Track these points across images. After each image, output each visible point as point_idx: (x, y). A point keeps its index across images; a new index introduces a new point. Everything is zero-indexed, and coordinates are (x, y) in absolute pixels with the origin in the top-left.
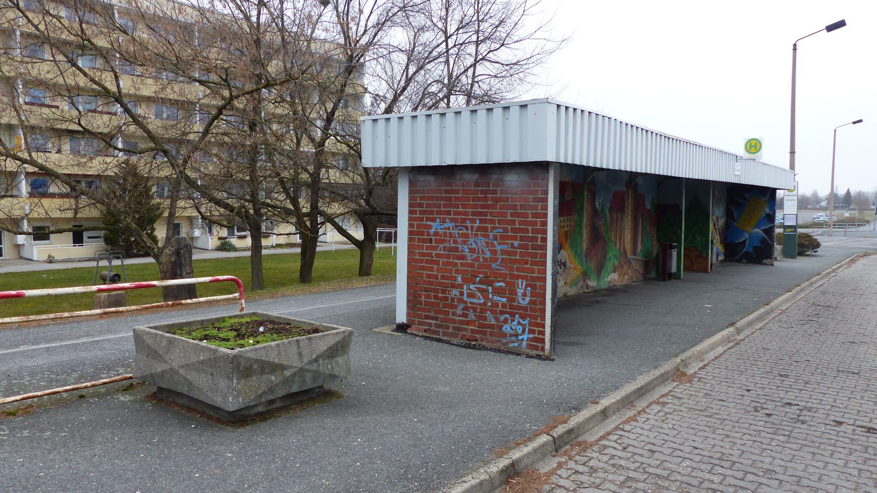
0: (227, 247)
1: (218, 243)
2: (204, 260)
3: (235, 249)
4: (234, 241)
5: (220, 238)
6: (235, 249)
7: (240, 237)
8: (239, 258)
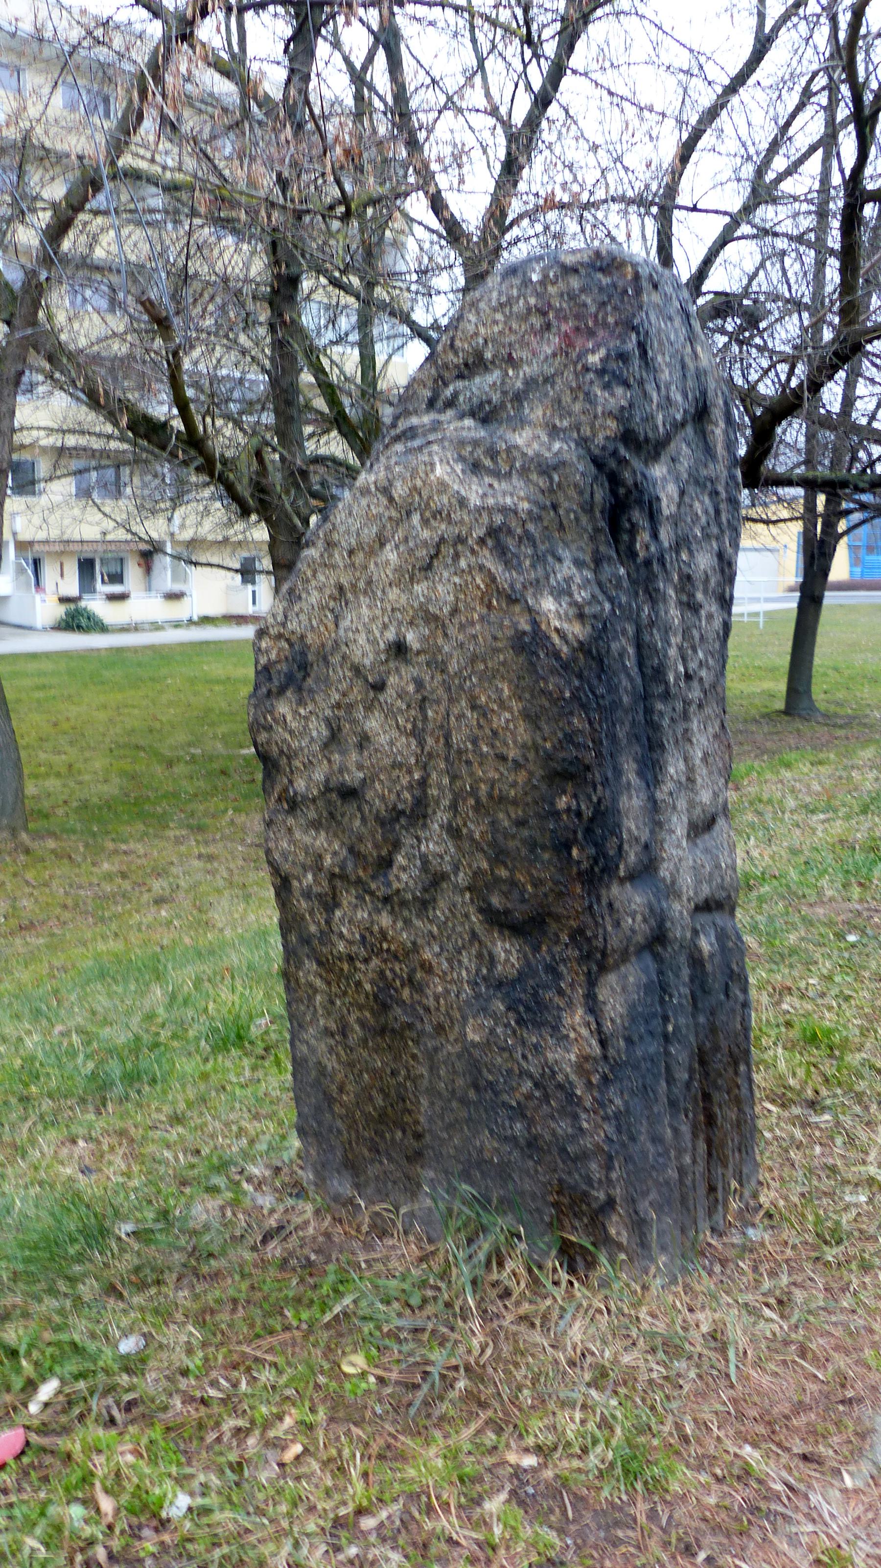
0: (84, 622)
1: (60, 611)
2: (33, 656)
3: (102, 628)
4: (96, 605)
5: (63, 600)
6: (102, 628)
7: (113, 598)
8: (119, 651)
